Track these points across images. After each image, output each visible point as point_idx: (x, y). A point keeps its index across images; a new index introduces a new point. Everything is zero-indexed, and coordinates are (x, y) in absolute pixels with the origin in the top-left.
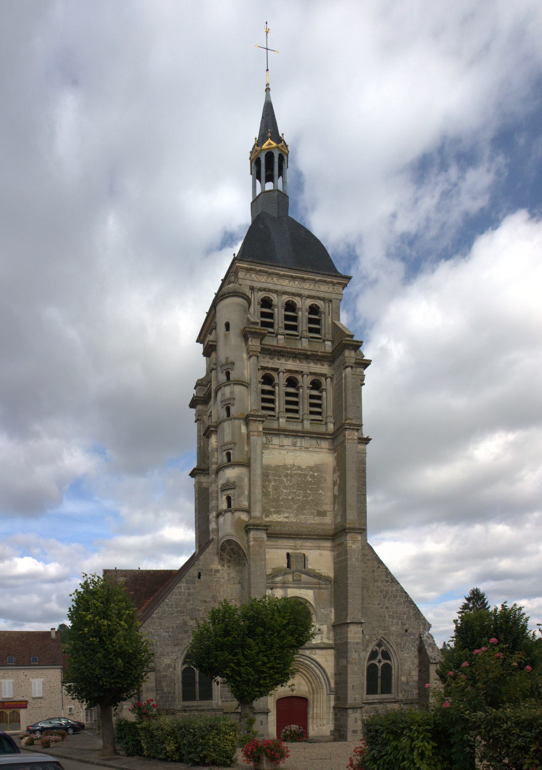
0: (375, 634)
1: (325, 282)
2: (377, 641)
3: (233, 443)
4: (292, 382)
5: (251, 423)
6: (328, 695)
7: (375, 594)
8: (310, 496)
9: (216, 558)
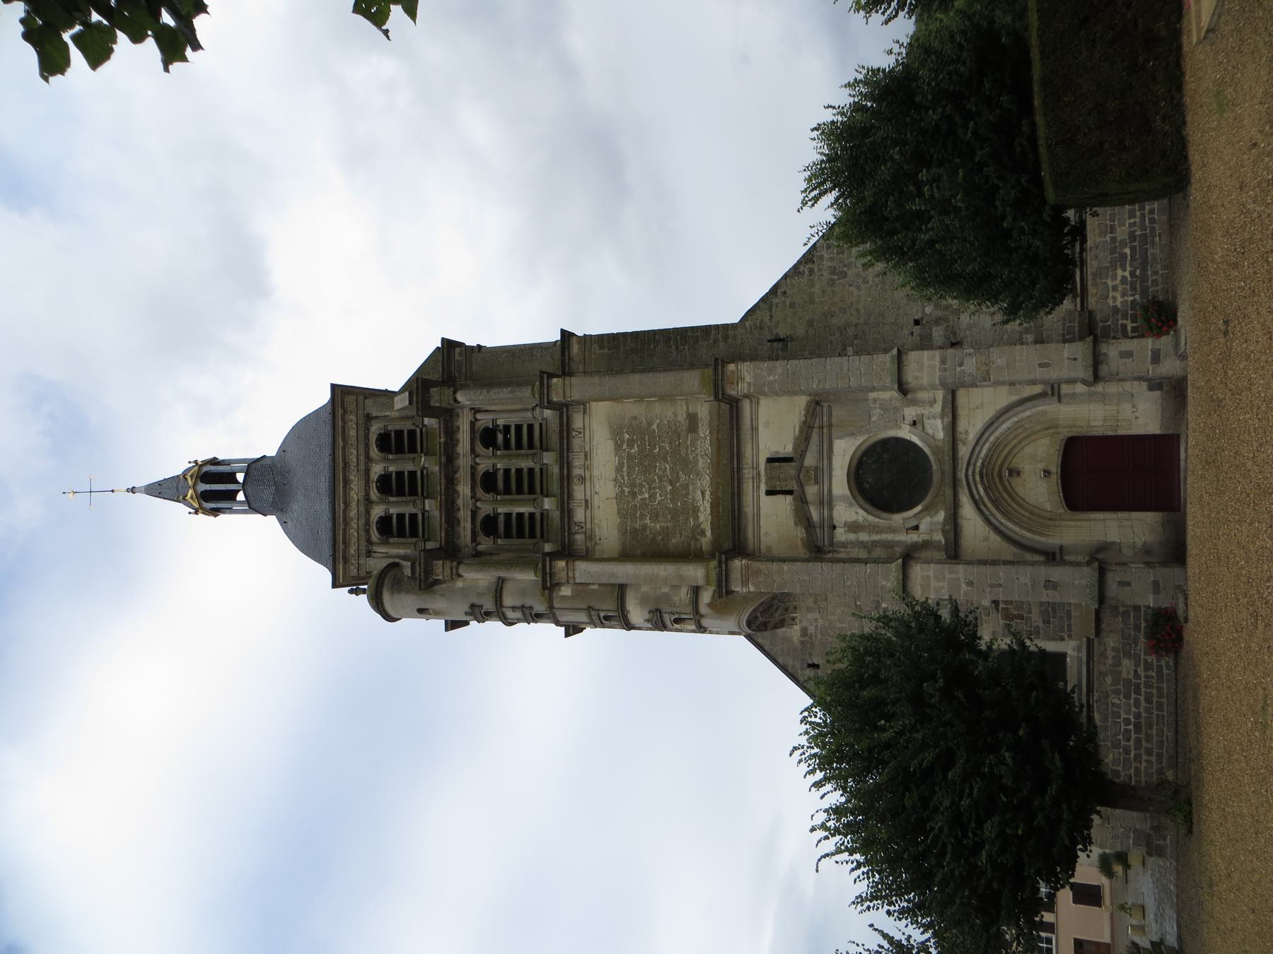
1: (343, 428)
7: (837, 300)
8: (664, 448)
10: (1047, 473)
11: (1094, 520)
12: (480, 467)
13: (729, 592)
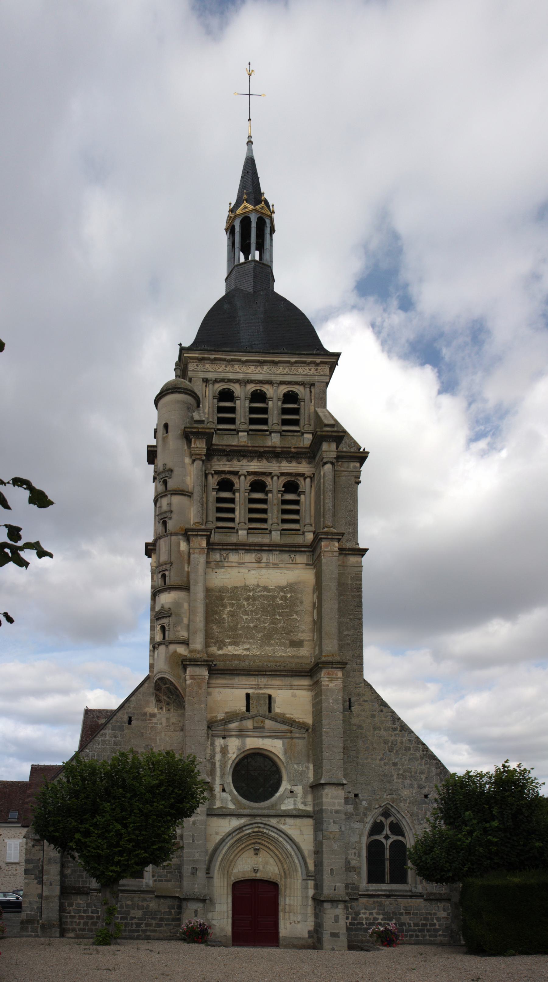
0: (377, 800)
1: (304, 362)
2: (381, 809)
3: (169, 563)
4: (258, 486)
5: (191, 538)
6: (303, 880)
7: (375, 745)
8: (280, 623)
9: (153, 699)
10: (256, 871)
11: (227, 897)
12: (269, 479)
13: (185, 667)
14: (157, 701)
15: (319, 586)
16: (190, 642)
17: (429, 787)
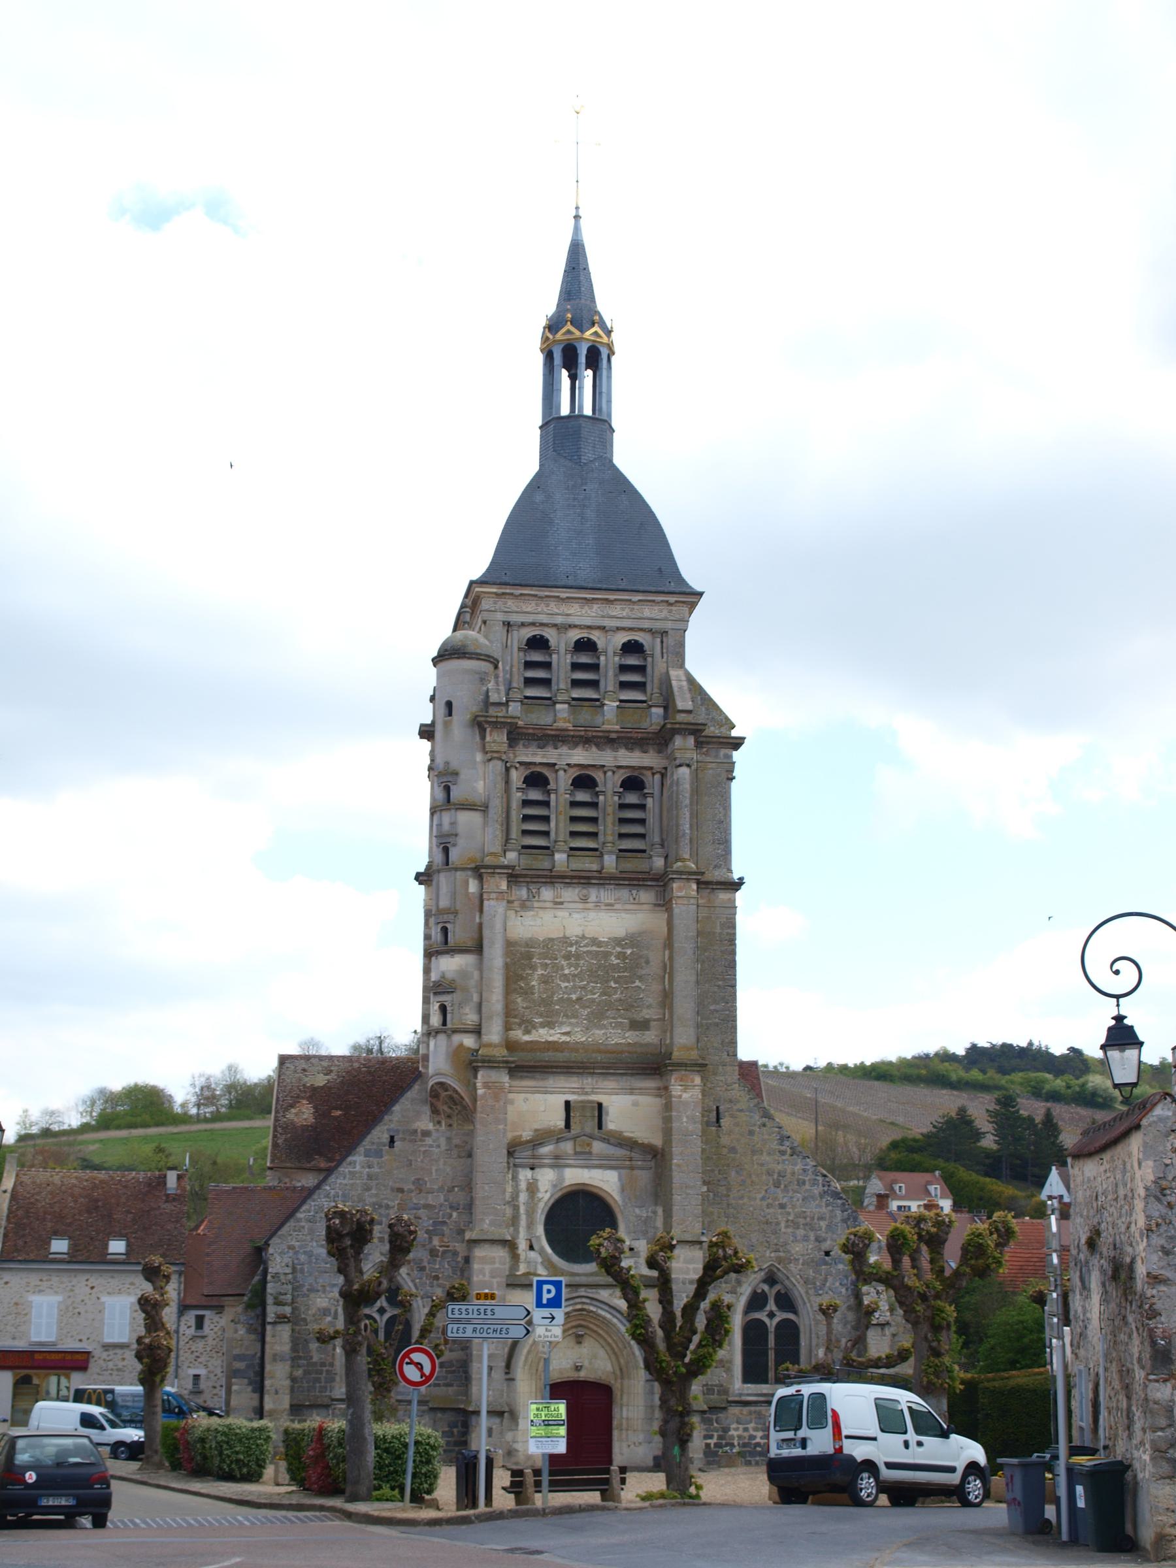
2: (763, 1273)
7: (754, 1177)
8: (615, 993)
9: (427, 1109)
10: (578, 1368)
13: (475, 1070)
14: (433, 1112)
15: (669, 943)
16: (483, 1031)
17: (832, 1240)
